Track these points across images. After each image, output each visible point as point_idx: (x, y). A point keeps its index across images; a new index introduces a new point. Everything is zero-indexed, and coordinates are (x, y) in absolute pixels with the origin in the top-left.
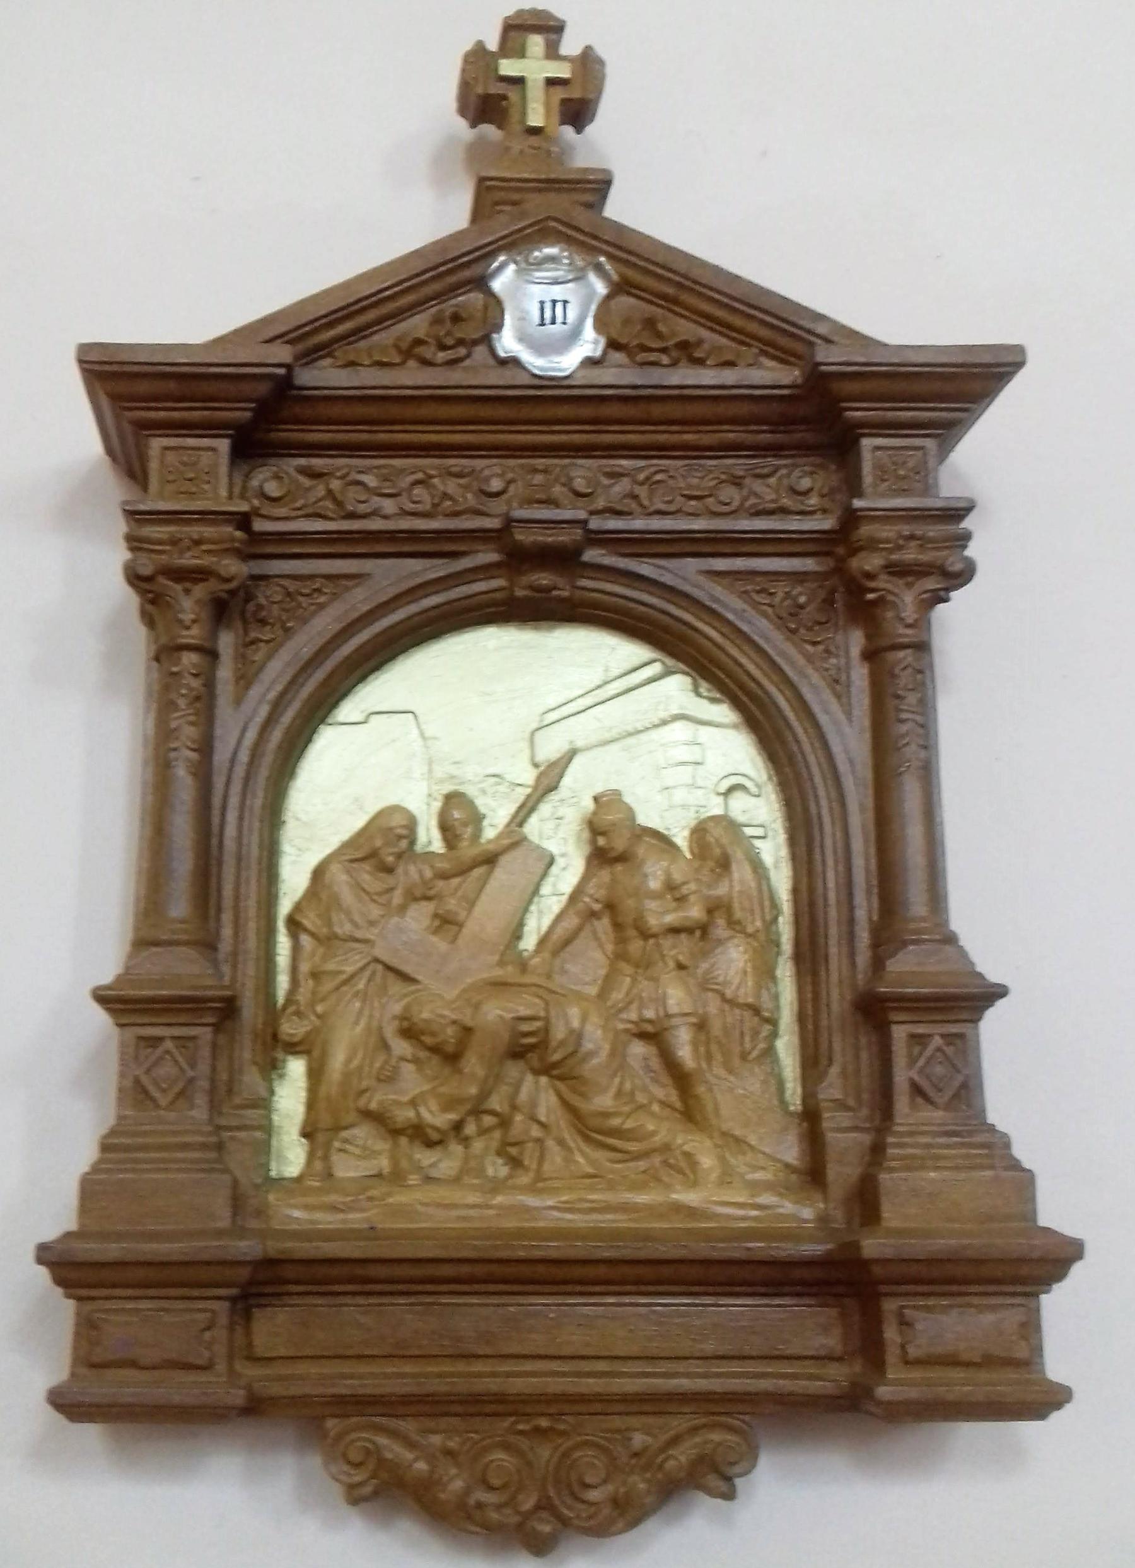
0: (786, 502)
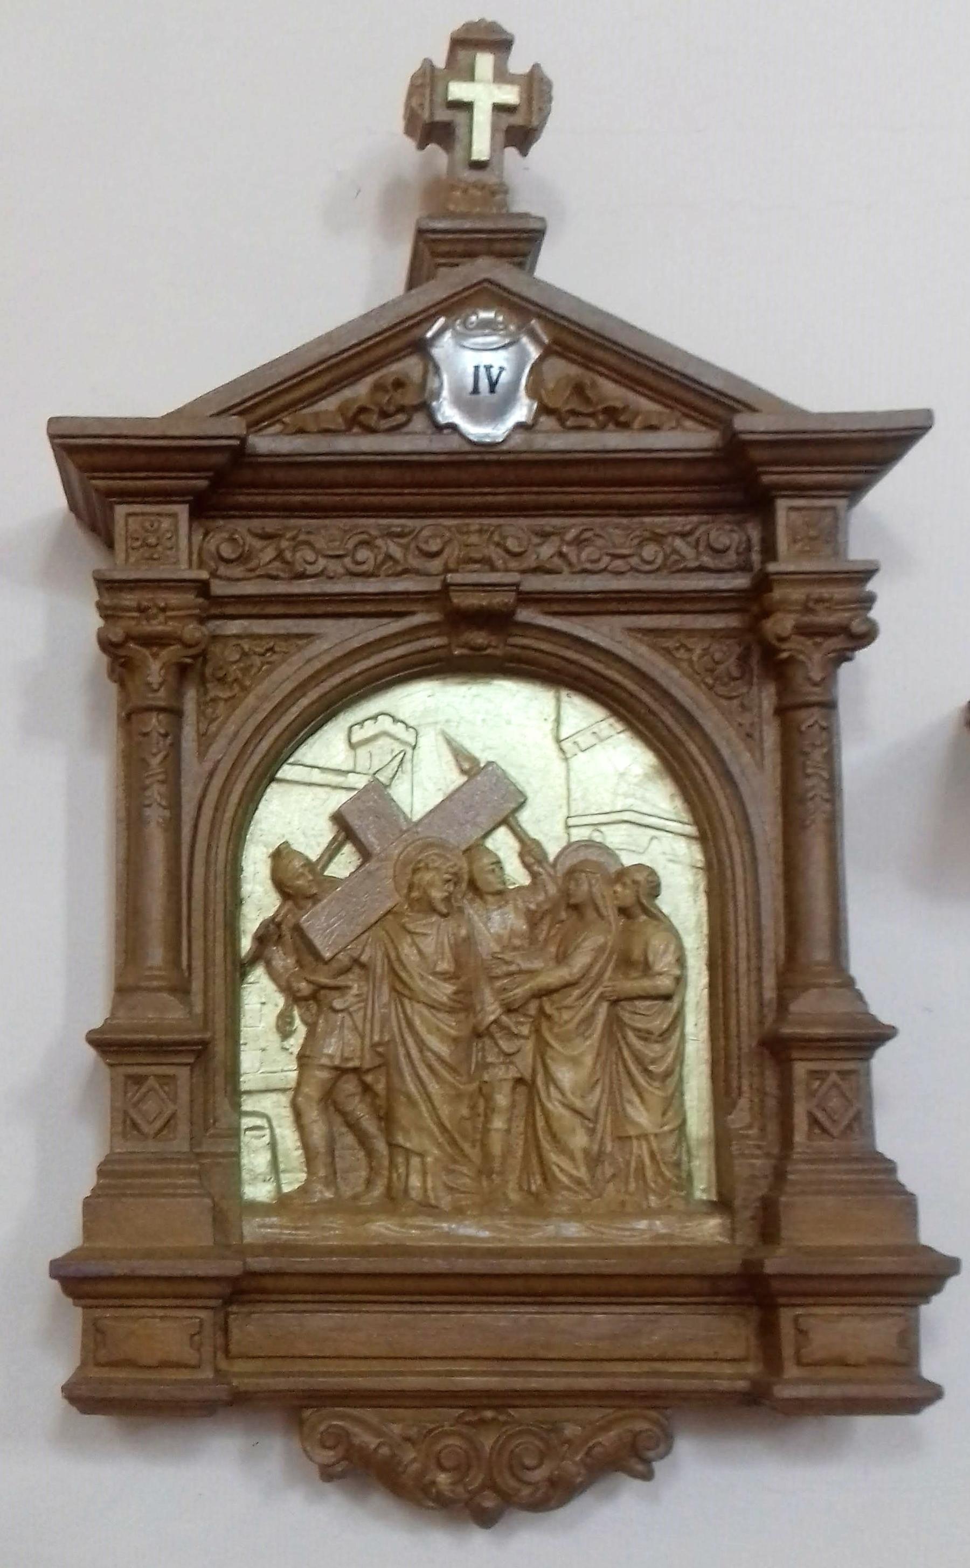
0: (706, 560)
